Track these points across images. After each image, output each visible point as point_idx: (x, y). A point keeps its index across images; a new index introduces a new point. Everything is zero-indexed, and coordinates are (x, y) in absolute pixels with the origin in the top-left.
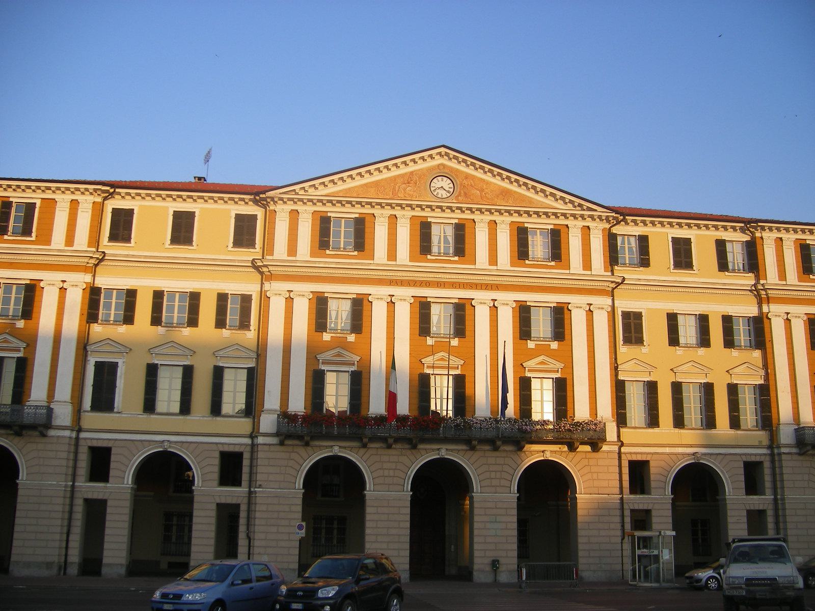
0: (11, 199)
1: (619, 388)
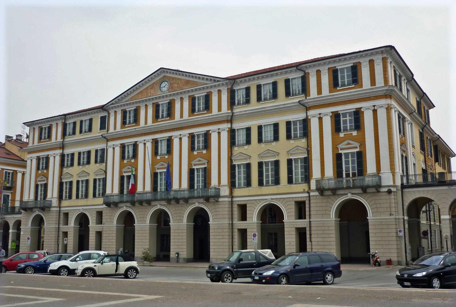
0: (337, 68)
1: (232, 168)
